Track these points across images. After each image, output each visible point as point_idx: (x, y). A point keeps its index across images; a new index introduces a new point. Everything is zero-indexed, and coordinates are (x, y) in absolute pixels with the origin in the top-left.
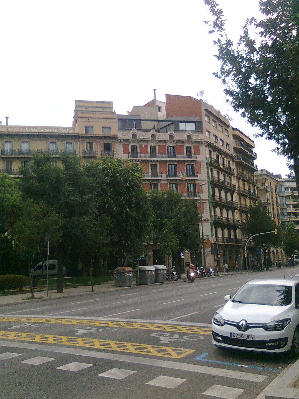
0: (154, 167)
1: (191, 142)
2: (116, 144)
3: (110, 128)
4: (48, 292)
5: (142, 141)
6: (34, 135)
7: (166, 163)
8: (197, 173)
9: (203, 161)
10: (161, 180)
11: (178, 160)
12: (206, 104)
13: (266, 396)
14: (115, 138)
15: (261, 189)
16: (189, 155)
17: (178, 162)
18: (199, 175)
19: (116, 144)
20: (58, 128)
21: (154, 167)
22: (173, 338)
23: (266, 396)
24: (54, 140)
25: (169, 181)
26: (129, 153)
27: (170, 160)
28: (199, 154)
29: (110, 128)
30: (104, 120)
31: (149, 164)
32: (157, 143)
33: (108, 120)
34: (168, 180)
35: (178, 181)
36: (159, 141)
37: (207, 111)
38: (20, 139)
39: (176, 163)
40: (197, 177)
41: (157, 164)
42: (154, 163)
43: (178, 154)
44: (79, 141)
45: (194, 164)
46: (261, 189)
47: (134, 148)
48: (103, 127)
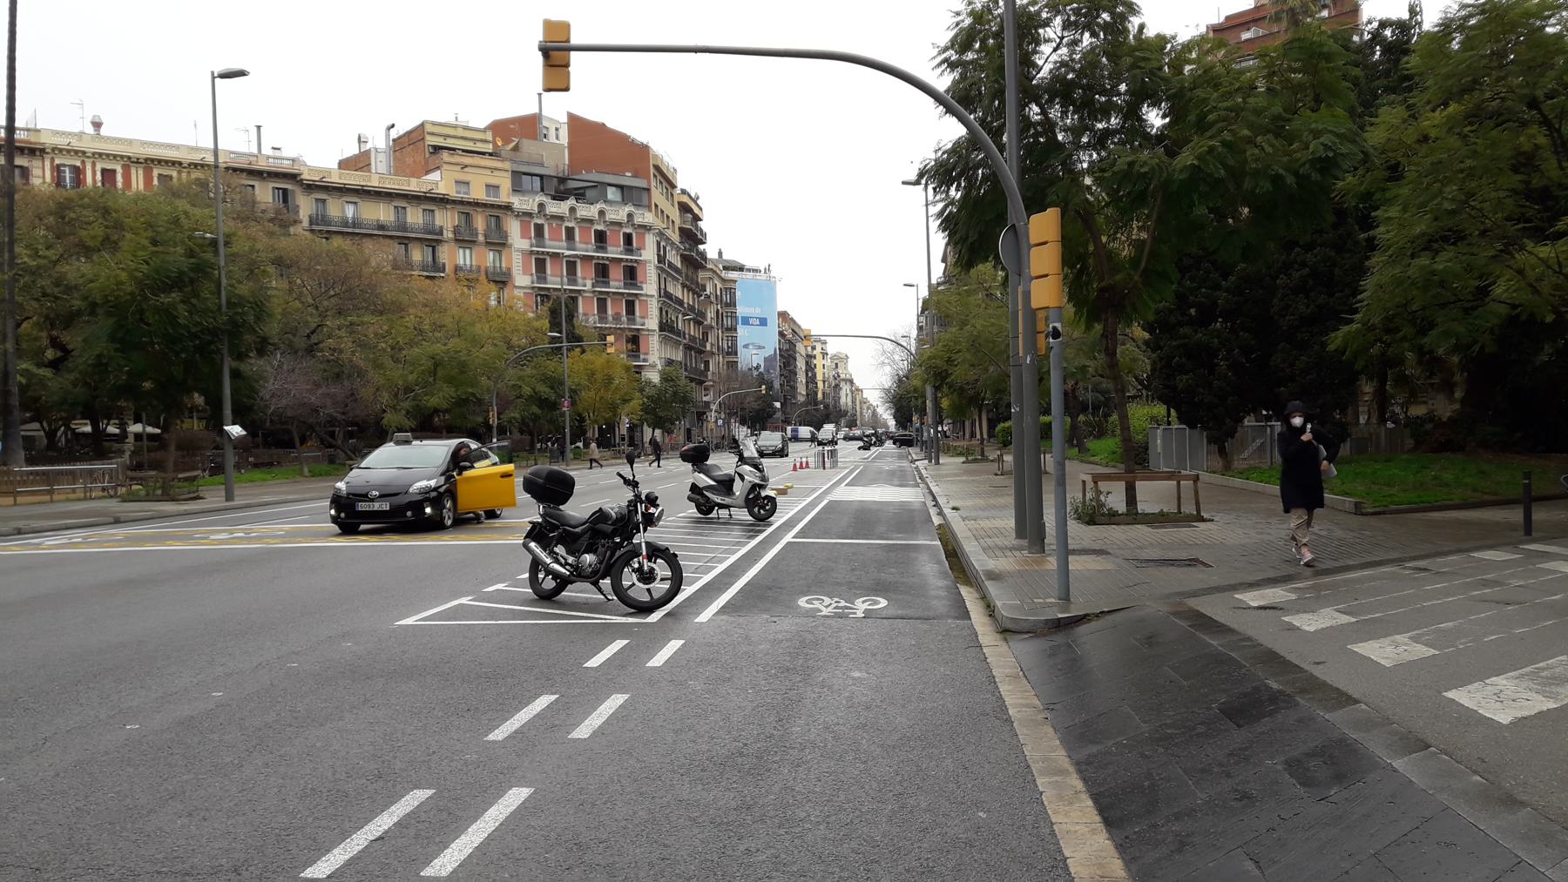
0: (571, 266)
1: (545, 215)
2: (509, 219)
3: (468, 183)
4: (18, 498)
5: (554, 217)
6: (369, 192)
7: (592, 260)
8: (642, 282)
9: (650, 262)
10: (584, 290)
11: (613, 258)
12: (656, 156)
13: (1287, 511)
14: (508, 208)
15: (1038, 333)
16: (629, 251)
17: (610, 261)
18: (644, 286)
19: (509, 219)
20: (130, 142)
21: (571, 266)
22: (930, 503)
23: (1287, 511)
24: (403, 204)
25: (536, 290)
26: (530, 238)
27: (598, 257)
28: (645, 249)
29: (468, 183)
30: (488, 172)
31: (565, 260)
32: (548, 219)
33: (496, 173)
34: (533, 288)
35: (551, 291)
36: (611, 222)
37: (657, 168)
38: (312, 193)
39: (607, 263)
40: (642, 289)
41: (545, 259)
42: (541, 257)
43: (610, 246)
44: (446, 208)
45: (635, 265)
46: (1038, 333)
47: (539, 229)
48: (457, 182)
